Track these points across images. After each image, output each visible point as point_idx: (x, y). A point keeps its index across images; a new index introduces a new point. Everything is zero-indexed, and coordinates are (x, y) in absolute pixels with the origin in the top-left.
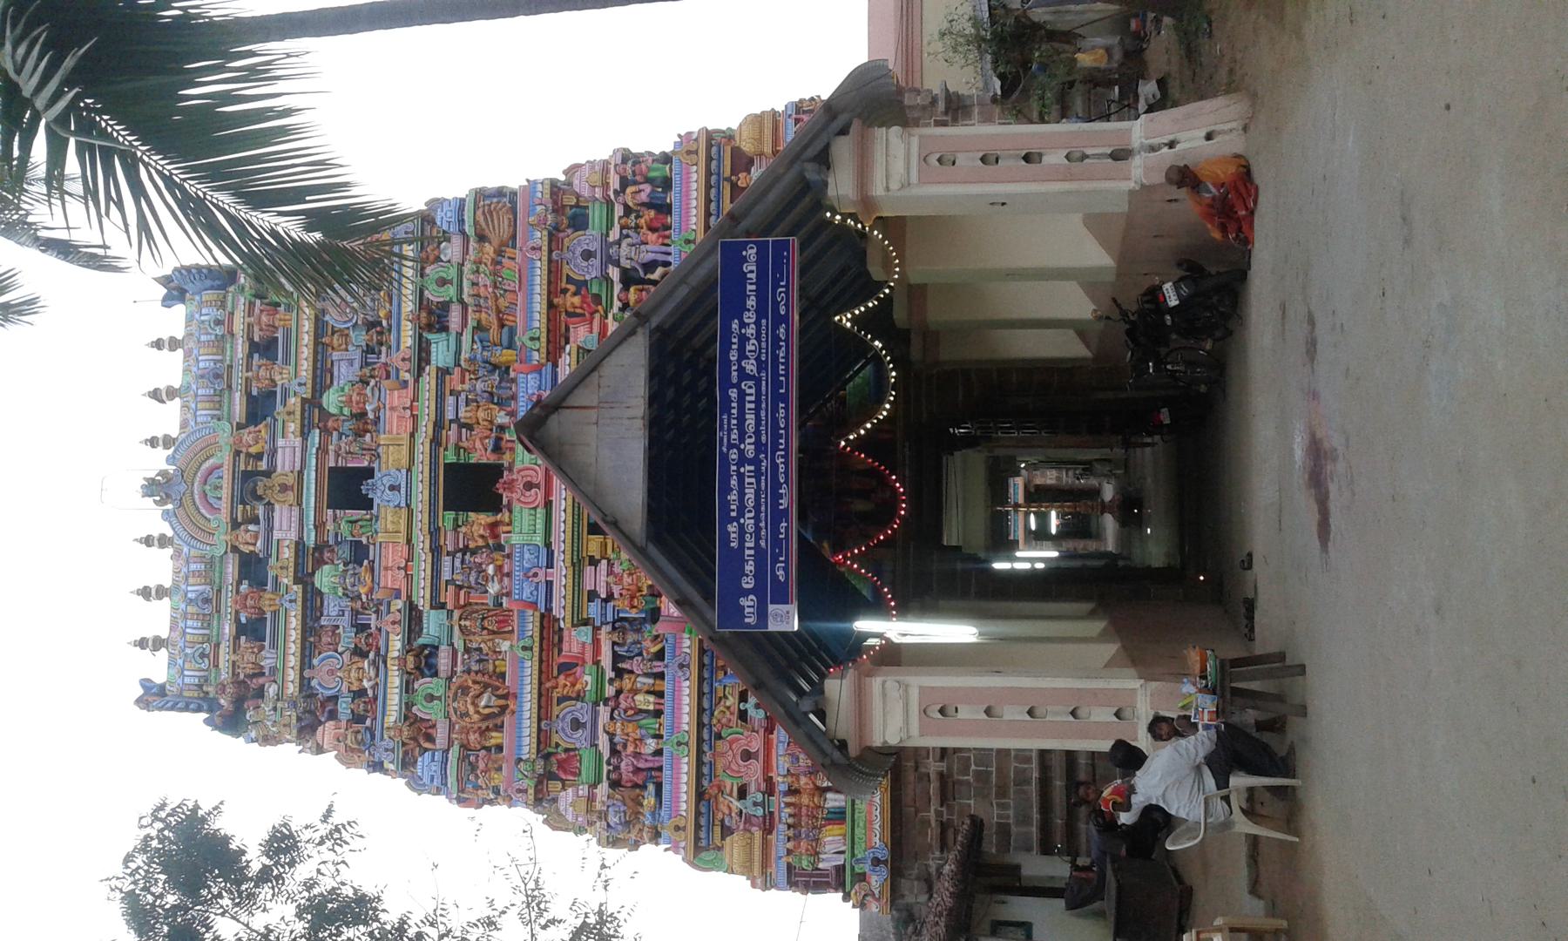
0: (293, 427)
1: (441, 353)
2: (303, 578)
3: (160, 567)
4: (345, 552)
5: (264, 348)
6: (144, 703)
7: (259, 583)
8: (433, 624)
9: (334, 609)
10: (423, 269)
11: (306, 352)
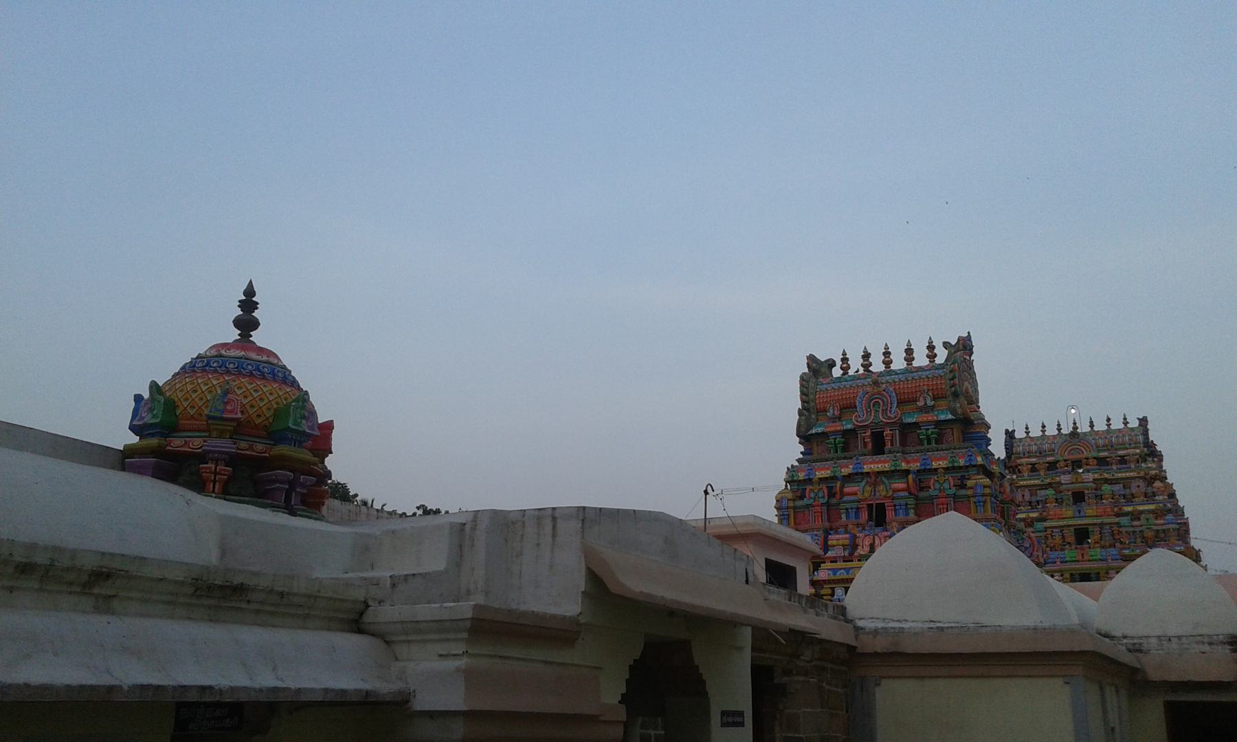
0: (1096, 476)
1: (1124, 520)
2: (1050, 485)
3: (1051, 431)
4: (1059, 496)
5: (1123, 460)
6: (1007, 432)
7: (1049, 469)
8: (1039, 526)
9: (1042, 493)
10: (826, 540)
11: (1124, 475)
